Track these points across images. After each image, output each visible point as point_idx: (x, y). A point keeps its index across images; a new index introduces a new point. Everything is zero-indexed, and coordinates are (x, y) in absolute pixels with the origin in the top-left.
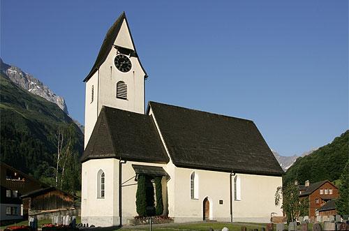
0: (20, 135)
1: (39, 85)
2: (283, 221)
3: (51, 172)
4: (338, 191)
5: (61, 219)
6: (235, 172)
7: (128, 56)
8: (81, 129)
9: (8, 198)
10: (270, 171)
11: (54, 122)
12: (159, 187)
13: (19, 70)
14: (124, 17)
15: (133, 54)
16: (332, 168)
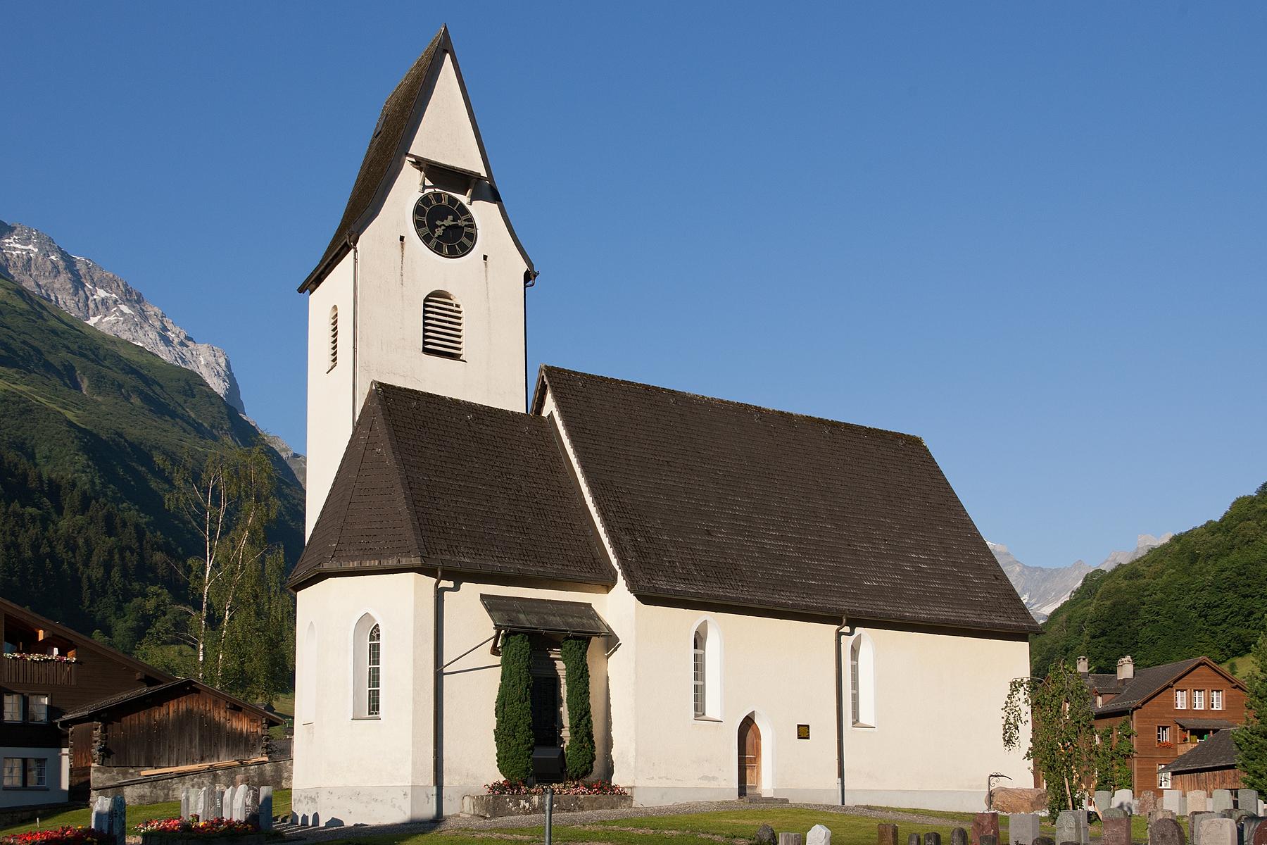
0: (59, 487)
1: (128, 301)
2: (1036, 804)
3: (181, 625)
4: (1246, 699)
5: (215, 798)
6: (855, 623)
7: (464, 199)
8: (294, 467)
9: (12, 726)
10: (760, 595)
11: (190, 443)
12: (581, 676)
13: (48, 244)
14: (444, 47)
15: (487, 190)
16: (1221, 613)
